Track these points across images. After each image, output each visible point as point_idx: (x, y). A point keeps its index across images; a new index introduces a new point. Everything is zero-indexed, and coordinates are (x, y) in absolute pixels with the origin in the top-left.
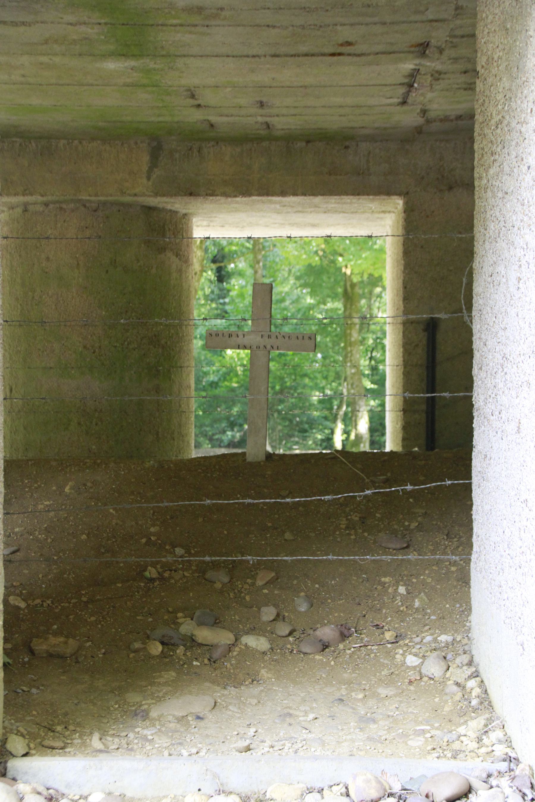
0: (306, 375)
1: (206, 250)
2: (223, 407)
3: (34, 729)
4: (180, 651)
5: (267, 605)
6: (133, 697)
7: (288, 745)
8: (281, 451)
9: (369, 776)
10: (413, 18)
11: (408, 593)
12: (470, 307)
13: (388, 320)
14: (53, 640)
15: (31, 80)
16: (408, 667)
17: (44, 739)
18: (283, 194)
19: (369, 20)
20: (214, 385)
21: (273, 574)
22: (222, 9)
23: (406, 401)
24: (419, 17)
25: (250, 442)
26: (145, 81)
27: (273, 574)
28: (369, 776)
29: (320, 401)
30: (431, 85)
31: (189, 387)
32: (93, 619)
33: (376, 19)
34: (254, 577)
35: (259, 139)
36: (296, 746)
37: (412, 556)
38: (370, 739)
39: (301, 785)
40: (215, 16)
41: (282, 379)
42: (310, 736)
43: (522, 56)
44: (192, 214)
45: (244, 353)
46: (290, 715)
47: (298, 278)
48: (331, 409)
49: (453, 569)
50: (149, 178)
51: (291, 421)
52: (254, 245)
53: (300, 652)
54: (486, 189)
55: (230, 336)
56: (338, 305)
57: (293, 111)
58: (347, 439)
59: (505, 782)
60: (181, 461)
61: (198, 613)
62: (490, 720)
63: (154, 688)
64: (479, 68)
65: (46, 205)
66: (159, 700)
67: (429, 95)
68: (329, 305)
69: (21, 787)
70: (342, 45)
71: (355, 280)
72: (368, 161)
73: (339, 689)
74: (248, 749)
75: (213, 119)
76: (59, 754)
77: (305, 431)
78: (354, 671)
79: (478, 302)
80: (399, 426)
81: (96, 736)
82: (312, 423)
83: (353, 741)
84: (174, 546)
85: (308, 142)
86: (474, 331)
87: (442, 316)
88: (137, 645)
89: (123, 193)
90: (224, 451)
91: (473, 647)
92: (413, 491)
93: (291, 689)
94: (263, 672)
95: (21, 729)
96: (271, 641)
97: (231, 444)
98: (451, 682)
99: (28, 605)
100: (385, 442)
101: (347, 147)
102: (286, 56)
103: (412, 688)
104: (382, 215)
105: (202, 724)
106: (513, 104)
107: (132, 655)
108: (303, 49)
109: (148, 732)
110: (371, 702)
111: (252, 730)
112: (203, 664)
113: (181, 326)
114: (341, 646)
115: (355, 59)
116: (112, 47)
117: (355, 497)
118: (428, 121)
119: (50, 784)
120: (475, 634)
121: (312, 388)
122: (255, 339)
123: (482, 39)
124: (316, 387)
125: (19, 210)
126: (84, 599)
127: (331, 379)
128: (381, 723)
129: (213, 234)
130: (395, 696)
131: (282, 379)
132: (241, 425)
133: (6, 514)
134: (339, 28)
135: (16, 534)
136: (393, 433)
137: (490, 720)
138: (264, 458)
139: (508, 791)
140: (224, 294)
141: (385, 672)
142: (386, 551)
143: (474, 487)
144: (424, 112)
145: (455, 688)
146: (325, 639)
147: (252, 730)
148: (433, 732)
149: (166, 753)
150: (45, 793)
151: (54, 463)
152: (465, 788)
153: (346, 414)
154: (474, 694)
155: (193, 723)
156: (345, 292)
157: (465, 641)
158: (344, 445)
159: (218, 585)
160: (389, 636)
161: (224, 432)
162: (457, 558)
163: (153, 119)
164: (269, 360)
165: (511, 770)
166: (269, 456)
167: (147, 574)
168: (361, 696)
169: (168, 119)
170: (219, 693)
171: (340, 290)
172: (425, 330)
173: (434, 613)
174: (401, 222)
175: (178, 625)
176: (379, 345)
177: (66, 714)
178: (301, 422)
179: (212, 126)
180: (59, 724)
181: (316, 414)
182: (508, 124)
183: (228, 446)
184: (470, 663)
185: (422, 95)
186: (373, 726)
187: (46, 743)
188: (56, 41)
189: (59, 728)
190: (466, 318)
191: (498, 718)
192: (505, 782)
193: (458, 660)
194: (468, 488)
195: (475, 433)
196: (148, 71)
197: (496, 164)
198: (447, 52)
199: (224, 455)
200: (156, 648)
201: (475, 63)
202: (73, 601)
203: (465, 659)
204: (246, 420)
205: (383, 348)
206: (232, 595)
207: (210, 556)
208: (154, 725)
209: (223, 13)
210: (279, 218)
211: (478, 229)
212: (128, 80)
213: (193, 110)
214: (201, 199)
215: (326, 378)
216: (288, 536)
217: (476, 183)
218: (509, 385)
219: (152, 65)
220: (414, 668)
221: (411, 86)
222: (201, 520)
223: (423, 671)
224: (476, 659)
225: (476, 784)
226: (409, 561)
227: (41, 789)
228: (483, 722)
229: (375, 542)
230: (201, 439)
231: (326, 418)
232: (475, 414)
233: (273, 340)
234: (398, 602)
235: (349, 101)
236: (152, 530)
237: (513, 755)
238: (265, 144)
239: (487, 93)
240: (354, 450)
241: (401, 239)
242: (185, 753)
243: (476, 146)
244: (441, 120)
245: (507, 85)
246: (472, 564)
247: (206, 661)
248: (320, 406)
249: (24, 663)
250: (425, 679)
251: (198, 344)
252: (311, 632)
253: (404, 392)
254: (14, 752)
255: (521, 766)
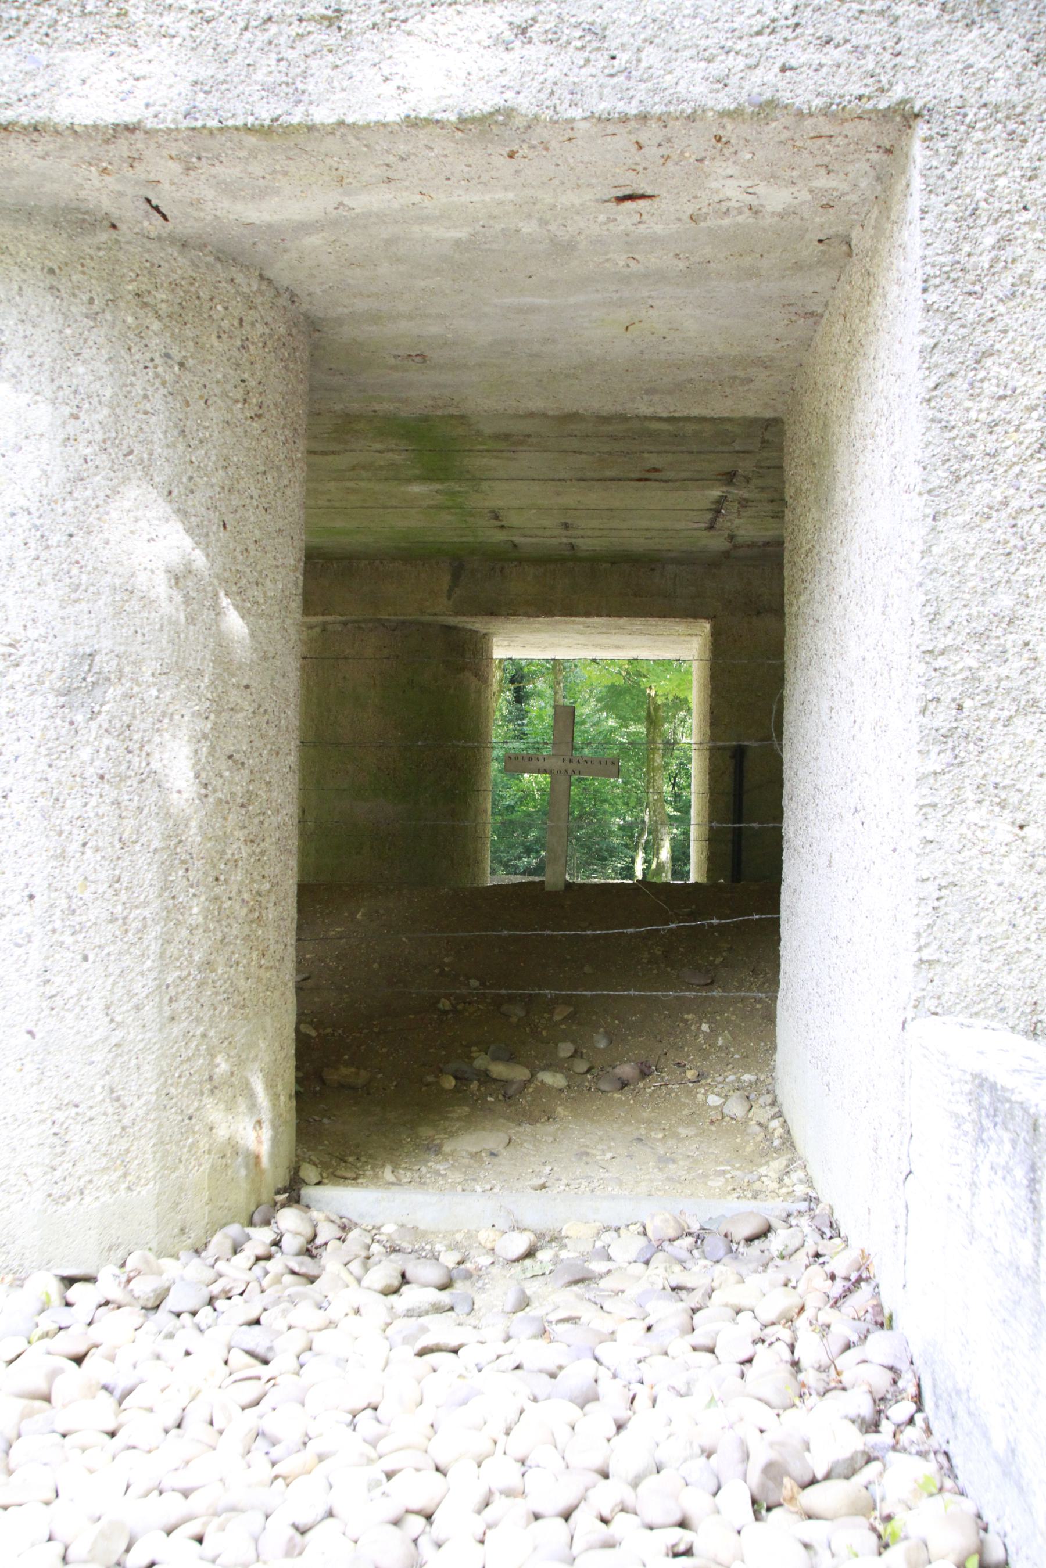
0: (605, 801)
1: (505, 670)
4: (474, 1086)
5: (564, 1041)
6: (426, 1132)
7: (584, 1184)
9: (668, 1216)
10: (720, 448)
11: (711, 1030)
13: (694, 746)
14: (344, 1071)
15: (337, 504)
17: (336, 1169)
18: (587, 614)
19: (675, 448)
20: (510, 809)
22: (529, 436)
23: (711, 829)
24: (724, 448)
25: (549, 870)
26: (450, 503)
28: (668, 1216)
29: (621, 828)
31: (485, 811)
32: (384, 1050)
33: (684, 448)
34: (551, 1012)
35: (563, 560)
36: (592, 1186)
37: (717, 993)
38: (669, 1179)
39: (598, 1224)
40: (521, 443)
41: (581, 804)
43: (830, 489)
44: (493, 634)
45: (543, 779)
46: (587, 1154)
47: (599, 700)
48: (631, 836)
49: (758, 1006)
50: (449, 597)
51: (590, 848)
52: (554, 667)
53: (598, 1089)
54: (797, 616)
56: (642, 729)
57: (597, 533)
59: (804, 1221)
60: (477, 889)
61: (492, 1048)
62: (792, 1161)
63: (447, 1123)
64: (787, 498)
66: (452, 1135)
67: (737, 521)
68: (632, 728)
69: (315, 1214)
70: (648, 471)
73: (638, 1129)
74: (543, 1187)
75: (517, 540)
76: (352, 1185)
77: (605, 859)
78: (653, 1111)
79: (788, 730)
80: (704, 856)
81: (388, 1169)
82: (612, 851)
83: (651, 1181)
84: (468, 978)
85: (613, 563)
86: (785, 760)
88: (430, 1079)
89: (423, 612)
90: (518, 879)
92: (719, 925)
93: (588, 1128)
94: (560, 1109)
96: (568, 1078)
97: (527, 872)
98: (753, 1122)
100: (688, 872)
101: (653, 570)
102: (592, 480)
103: (713, 1128)
105: (496, 1160)
106: (823, 535)
108: (609, 473)
109: (441, 1167)
110: (671, 1142)
111: (548, 1168)
114: (641, 1085)
115: (663, 484)
116: (417, 472)
117: (658, 930)
118: (735, 547)
119: (343, 1213)
120: (779, 1073)
121: (612, 815)
122: (556, 764)
123: (789, 472)
124: (617, 813)
125: (318, 630)
126: (376, 1030)
127: (632, 804)
128: (681, 1163)
129: (515, 655)
132: (538, 852)
133: (298, 940)
134: (646, 455)
135: (307, 960)
136: (697, 863)
137: (792, 1161)
139: (807, 1230)
140: (522, 715)
141: (686, 1112)
142: (689, 987)
143: (782, 922)
144: (731, 537)
145: (758, 1129)
146: (625, 1077)
147: (548, 1168)
149: (459, 1188)
150: (338, 1221)
152: (764, 1227)
153: (647, 841)
154: (776, 1134)
155: (487, 1159)
157: (769, 1080)
158: (644, 874)
159: (514, 1020)
160: (690, 1074)
161: (520, 858)
162: (763, 996)
165: (811, 1209)
166: (569, 886)
167: (440, 1006)
168: (660, 1136)
169: (471, 539)
170: (513, 1130)
171: (643, 714)
173: (738, 1052)
174: (708, 645)
176: (683, 769)
177: (357, 1146)
178: (601, 849)
179: (515, 546)
181: (616, 841)
182: (818, 553)
183: (524, 873)
184: (773, 1103)
185: (730, 520)
186: (672, 1166)
187: (339, 1173)
188: (363, 468)
189: (351, 1159)
190: (776, 746)
191: (800, 1158)
192: (804, 1221)
193: (761, 1101)
194: (776, 924)
196: (453, 494)
197: (808, 592)
198: (755, 481)
199: (521, 884)
200: (449, 1083)
202: (365, 1031)
203: (769, 1099)
204: (543, 847)
205: (688, 775)
206: (528, 1030)
208: (447, 1160)
210: (582, 639)
211: (789, 656)
214: (502, 619)
215: (627, 804)
216: (587, 969)
217: (787, 610)
218: (821, 817)
219: (457, 488)
220: (716, 1108)
223: (725, 1111)
225: (775, 1223)
226: (713, 998)
227: (334, 1217)
231: (626, 846)
233: (574, 765)
235: (655, 524)
236: (446, 960)
237: (813, 1195)
238: (570, 564)
239: (796, 522)
240: (655, 880)
241: (708, 663)
242: (479, 1189)
243: (786, 573)
244: (749, 546)
247: (501, 1097)
248: (621, 833)
249: (315, 1093)
250: (727, 1119)
251: (495, 765)
252: (610, 1069)
253: (711, 822)
254: (307, 1179)
255: (821, 1206)
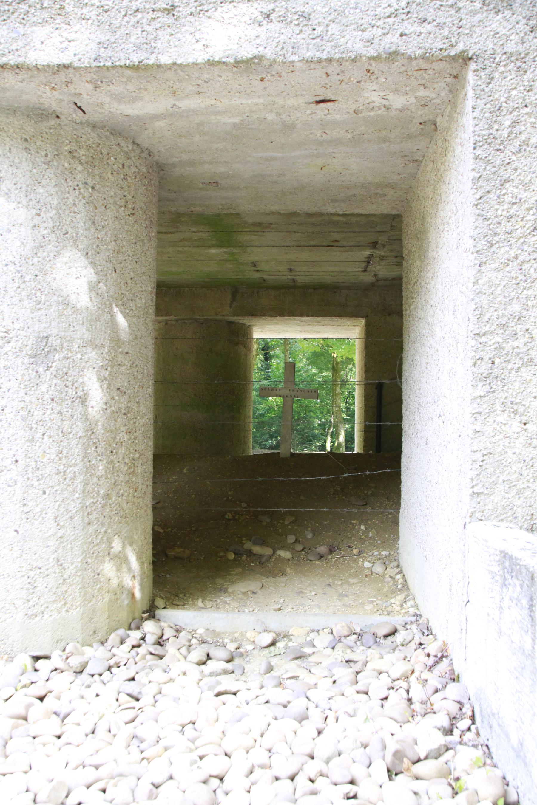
0: (311, 411)
1: (259, 344)
2: (267, 427)
3: (168, 595)
4: (244, 557)
6: (219, 581)
7: (301, 608)
8: (298, 452)
9: (344, 624)
11: (366, 529)
12: (401, 377)
14: (178, 550)
15: (173, 259)
16: (365, 568)
17: (173, 600)
18: (301, 315)
20: (262, 415)
21: (294, 518)
22: (271, 224)
25: (282, 447)
26: (231, 259)
27: (294, 518)
28: (344, 624)
30: (379, 263)
31: (249, 417)
32: (198, 539)
33: (350, 230)
34: (284, 520)
35: (289, 287)
36: (305, 609)
37: (369, 510)
38: (344, 605)
39: (308, 628)
41: (298, 413)
42: (313, 603)
44: (253, 325)
46: (302, 592)
47: (307, 359)
48: (324, 429)
49: (390, 516)
50: (230, 307)
51: (303, 435)
52: (285, 342)
53: (307, 559)
54: (409, 316)
55: (272, 390)
56: (329, 374)
58: (333, 445)
59: (414, 627)
60: (245, 456)
61: (254, 538)
62: (407, 596)
64: (404, 256)
65: (177, 321)
66: (233, 583)
67: (378, 267)
68: (325, 374)
69: (163, 624)
71: (339, 360)
72: (346, 300)
73: (328, 579)
74: (280, 609)
75: (265, 277)
76: (182, 609)
77: (311, 441)
78: (336, 570)
79: (405, 375)
80: (362, 439)
81: (200, 601)
82: (314, 437)
83: (335, 606)
84: (241, 502)
85: (314, 289)
87: (386, 381)
88: (221, 554)
89: (217, 315)
90: (266, 451)
91: (400, 558)
92: (369, 475)
93: (303, 579)
95: (162, 595)
96: (292, 553)
97: (271, 447)
99: (164, 532)
100: (354, 447)
101: (335, 292)
103: (367, 579)
104: (353, 327)
105: (255, 596)
107: (218, 559)
108: (313, 243)
109: (227, 600)
110: (345, 586)
111: (282, 600)
112: (256, 565)
113: (246, 384)
114: (330, 557)
115: (340, 248)
116: (214, 242)
118: (377, 280)
120: (401, 551)
121: (314, 418)
122: (286, 392)
123: (405, 243)
124: (317, 417)
125: (163, 324)
126: (193, 529)
127: (325, 413)
130: (358, 583)
131: (298, 413)
132: (276, 437)
133: (153, 483)
134: (332, 234)
135: (158, 493)
137: (407, 596)
138: (289, 455)
139: (415, 631)
140: (268, 367)
142: (354, 506)
143: (402, 473)
145: (390, 579)
146: (321, 553)
147: (282, 600)
148: (378, 602)
149: (237, 610)
150: (175, 627)
151: (178, 457)
152: (393, 630)
153: (333, 432)
154: (399, 582)
155: (251, 595)
156: (333, 367)
157: (396, 554)
158: (331, 449)
159: (264, 523)
160: (355, 551)
161: (267, 441)
162: (392, 511)
163: (233, 277)
164: (293, 403)
165: (417, 621)
166: (293, 455)
167: (226, 517)
168: (340, 583)
169: (241, 277)
170: (264, 580)
171: (330, 366)
172: (376, 389)
173: (379, 540)
175: (243, 544)
176: (351, 395)
177: (184, 589)
178: (309, 436)
179: (264, 280)
180: (181, 593)
182: (420, 284)
183: (269, 448)
184: (398, 566)
185: (375, 267)
186: (346, 599)
187: (175, 602)
188: (186, 241)
190: (399, 383)
191: (412, 594)
192: (414, 627)
193: (392, 565)
194: (399, 474)
195: (403, 444)
199: (268, 454)
200: (231, 556)
201: (402, 253)
203: (395, 564)
205: (354, 398)
207: (261, 507)
209: (272, 226)
210: (299, 328)
211: (405, 336)
212: (222, 258)
213: (255, 272)
215: (322, 413)
216: (302, 498)
217: (404, 313)
218: (422, 419)
219: (234, 251)
220: (368, 568)
221: (369, 262)
222: (255, 488)
223: (373, 570)
224: (401, 564)
225: (399, 628)
226: (366, 512)
227: (172, 625)
228: (404, 597)
229: (349, 502)
230: (255, 445)
231: (322, 434)
232: (403, 434)
233: (295, 393)
234: (360, 533)
236: (229, 493)
237: (419, 613)
240: (337, 451)
241: (364, 340)
242: (247, 611)
244: (384, 280)
245: (419, 265)
246: (400, 514)
247: (258, 563)
248: (319, 428)
250: (374, 574)
251: (254, 393)
252: (314, 549)
253: (365, 422)
255: (422, 619)
